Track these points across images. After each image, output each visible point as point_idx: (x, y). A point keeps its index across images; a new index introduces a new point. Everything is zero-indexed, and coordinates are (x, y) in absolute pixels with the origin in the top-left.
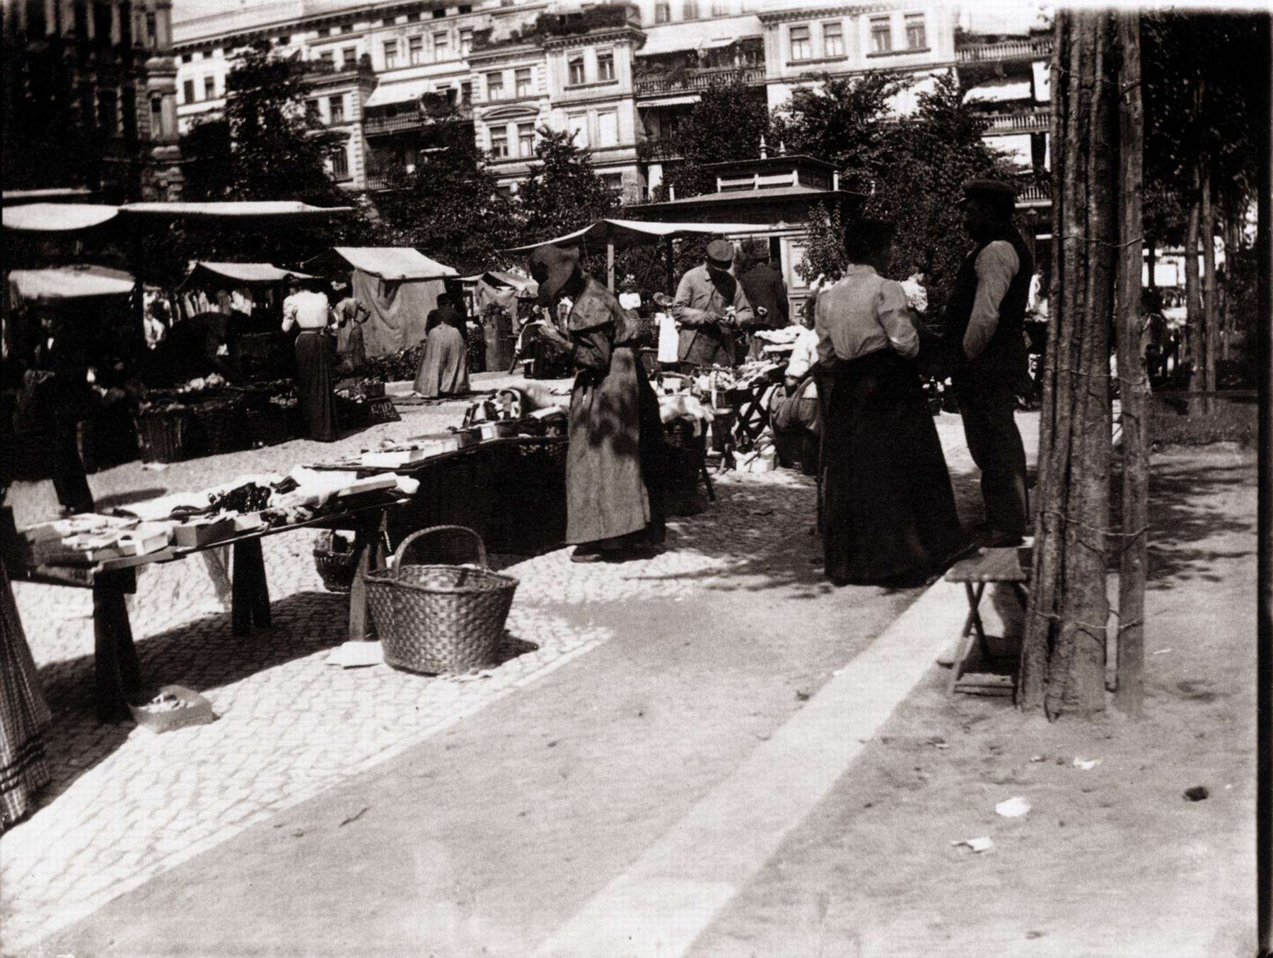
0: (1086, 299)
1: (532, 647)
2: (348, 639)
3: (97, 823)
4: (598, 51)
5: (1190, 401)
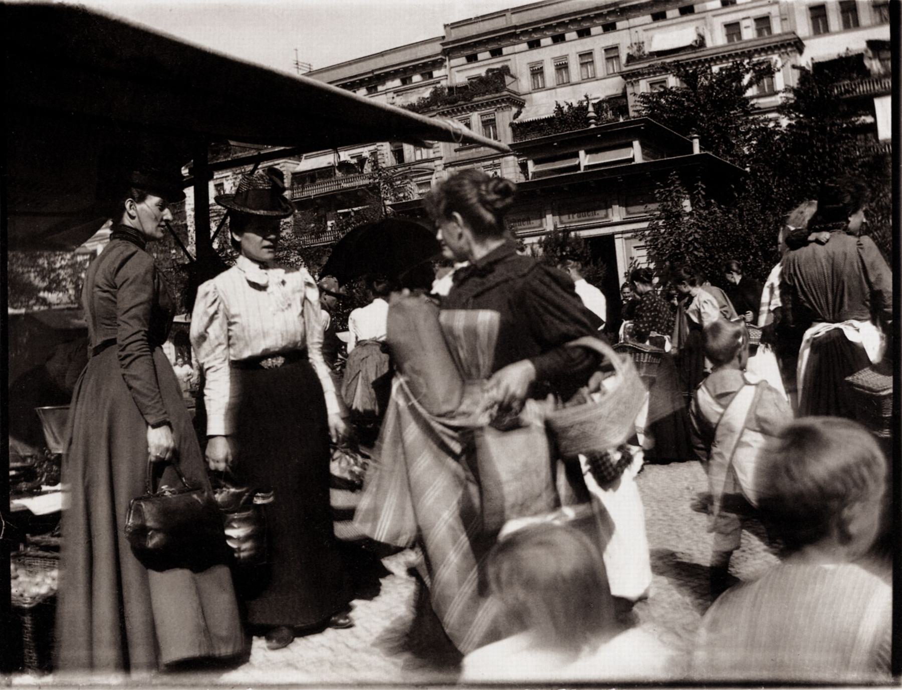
0: (771, 120)
1: (556, 102)
2: (384, 299)
3: (216, 304)
4: (482, 116)
5: (809, 68)
